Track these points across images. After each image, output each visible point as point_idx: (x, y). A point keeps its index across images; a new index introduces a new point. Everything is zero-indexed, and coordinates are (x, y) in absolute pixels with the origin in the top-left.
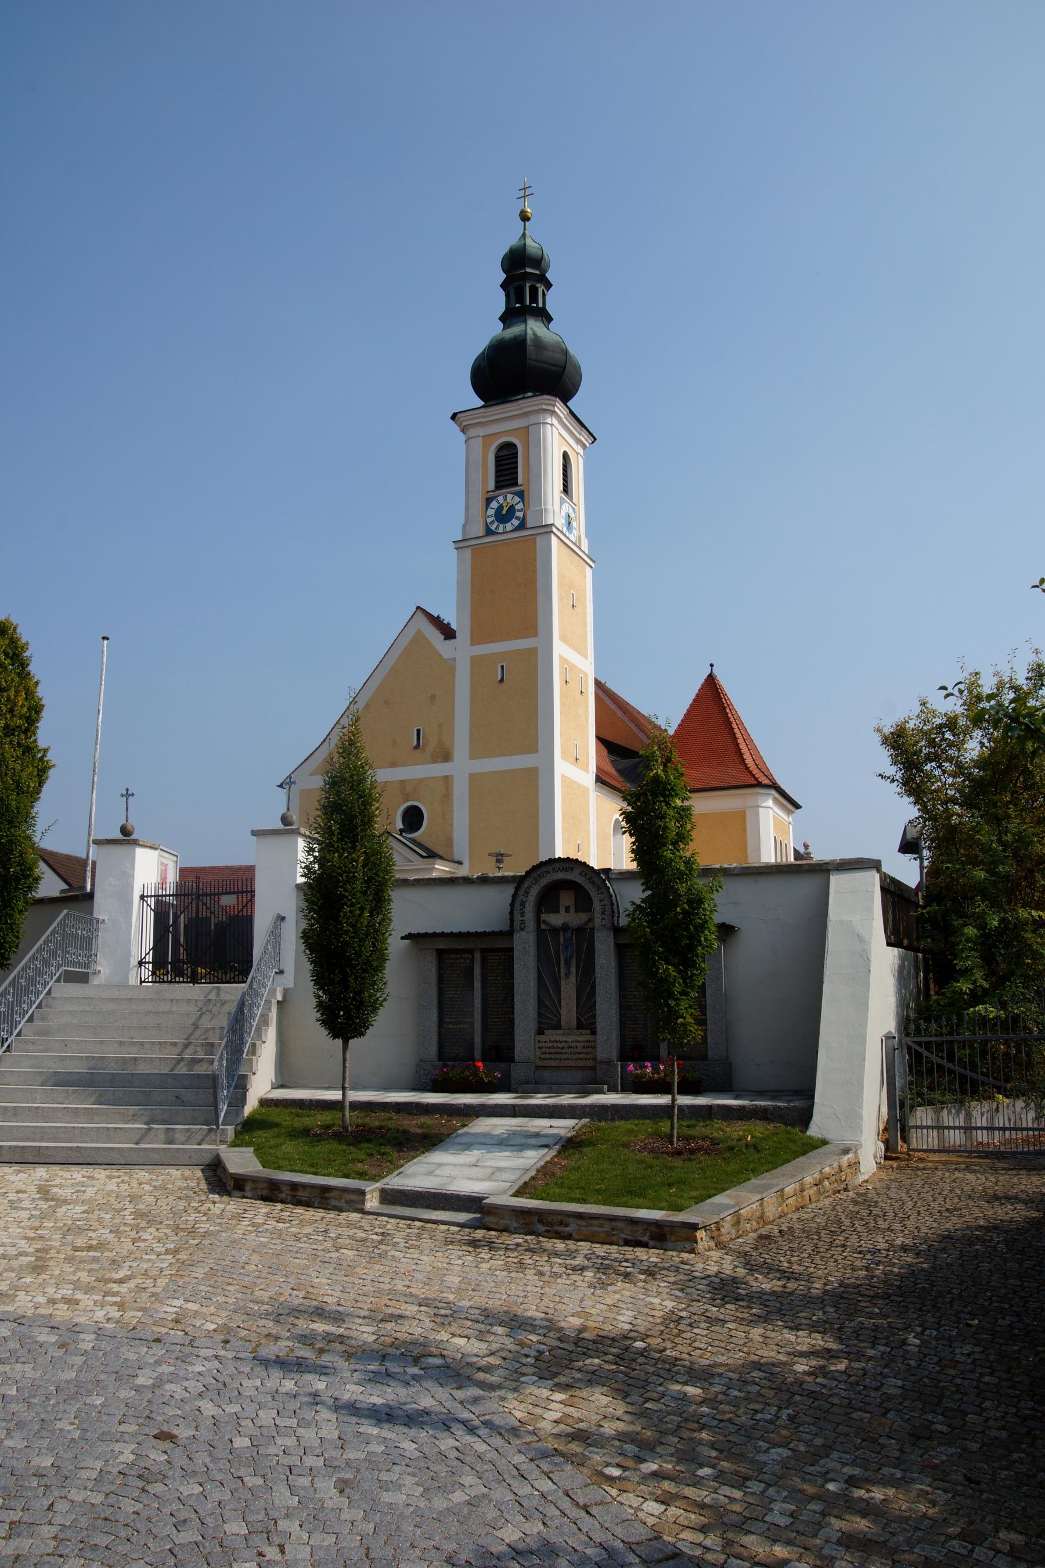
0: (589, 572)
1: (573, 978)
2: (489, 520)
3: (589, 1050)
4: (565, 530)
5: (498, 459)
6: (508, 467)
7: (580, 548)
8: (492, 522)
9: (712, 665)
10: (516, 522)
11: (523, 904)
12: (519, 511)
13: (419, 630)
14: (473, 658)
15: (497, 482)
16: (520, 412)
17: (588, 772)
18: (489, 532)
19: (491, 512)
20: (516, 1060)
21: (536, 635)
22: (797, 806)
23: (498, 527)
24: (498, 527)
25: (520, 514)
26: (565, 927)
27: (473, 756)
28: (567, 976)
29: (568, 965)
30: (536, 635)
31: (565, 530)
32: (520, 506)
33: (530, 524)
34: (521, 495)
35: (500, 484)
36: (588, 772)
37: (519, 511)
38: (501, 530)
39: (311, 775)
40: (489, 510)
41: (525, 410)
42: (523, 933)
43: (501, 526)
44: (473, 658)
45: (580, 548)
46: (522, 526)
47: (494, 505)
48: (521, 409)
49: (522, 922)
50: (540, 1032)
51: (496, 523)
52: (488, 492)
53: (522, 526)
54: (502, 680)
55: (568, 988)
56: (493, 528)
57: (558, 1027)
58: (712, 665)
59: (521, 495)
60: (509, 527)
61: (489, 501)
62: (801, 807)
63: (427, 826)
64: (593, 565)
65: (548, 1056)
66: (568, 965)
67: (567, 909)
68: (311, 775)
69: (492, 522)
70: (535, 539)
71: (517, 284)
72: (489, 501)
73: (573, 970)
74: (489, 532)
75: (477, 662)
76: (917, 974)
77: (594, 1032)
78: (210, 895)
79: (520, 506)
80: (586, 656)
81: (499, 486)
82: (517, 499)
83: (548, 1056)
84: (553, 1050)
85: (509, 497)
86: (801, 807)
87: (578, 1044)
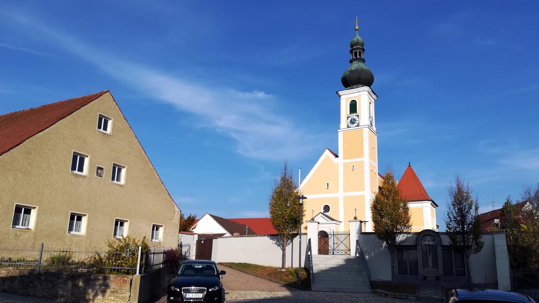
1: (431, 256)
2: (348, 123)
3: (437, 273)
4: (370, 126)
5: (351, 105)
9: (409, 163)
10: (357, 124)
11: (419, 239)
14: (363, 157)
16: (358, 91)
18: (348, 127)
19: (349, 121)
22: (437, 206)
25: (358, 122)
26: (429, 245)
27: (344, 191)
28: (430, 256)
29: (430, 253)
31: (370, 126)
32: (358, 119)
33: (361, 124)
34: (358, 116)
41: (359, 91)
42: (419, 246)
43: (352, 125)
44: (363, 157)
46: (358, 126)
47: (350, 119)
49: (419, 243)
50: (424, 268)
51: (350, 124)
53: (358, 126)
55: (430, 259)
56: (349, 126)
57: (428, 267)
58: (409, 163)
59: (358, 116)
60: (354, 125)
61: (348, 118)
62: (438, 206)
65: (426, 274)
66: (430, 253)
67: (429, 241)
70: (362, 131)
71: (355, 51)
72: (348, 118)
73: (431, 254)
74: (348, 127)
75: (345, 164)
77: (438, 269)
78: (337, 234)
82: (357, 117)
83: (426, 274)
84: (427, 272)
85: (354, 117)
86: (438, 206)
87: (434, 271)
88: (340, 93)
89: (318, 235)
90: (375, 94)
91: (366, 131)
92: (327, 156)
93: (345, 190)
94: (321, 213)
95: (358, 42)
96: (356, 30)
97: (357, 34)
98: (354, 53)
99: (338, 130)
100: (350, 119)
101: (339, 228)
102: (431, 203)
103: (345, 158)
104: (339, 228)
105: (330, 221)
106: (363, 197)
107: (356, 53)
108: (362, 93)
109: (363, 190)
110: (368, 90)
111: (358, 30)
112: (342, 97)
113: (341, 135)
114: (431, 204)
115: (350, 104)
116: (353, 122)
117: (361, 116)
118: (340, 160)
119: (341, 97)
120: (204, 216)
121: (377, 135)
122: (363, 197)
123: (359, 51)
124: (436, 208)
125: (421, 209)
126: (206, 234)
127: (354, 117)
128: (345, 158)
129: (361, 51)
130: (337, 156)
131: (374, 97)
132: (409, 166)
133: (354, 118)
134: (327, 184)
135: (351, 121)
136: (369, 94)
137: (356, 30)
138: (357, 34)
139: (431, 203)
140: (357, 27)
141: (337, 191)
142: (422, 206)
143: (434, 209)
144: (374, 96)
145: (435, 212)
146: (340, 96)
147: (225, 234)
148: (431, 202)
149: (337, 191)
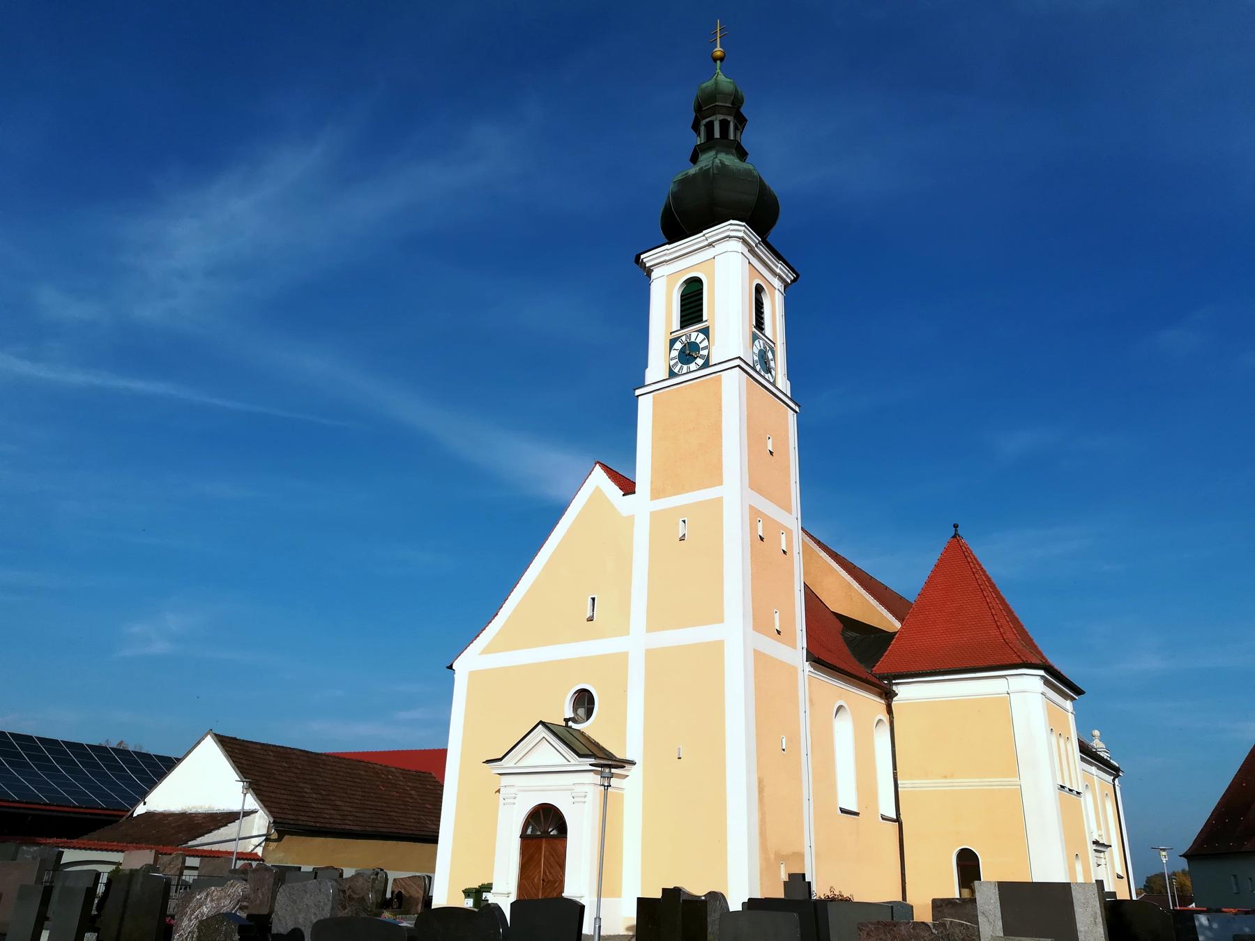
0: (792, 419)
2: (672, 363)
5: (684, 298)
6: (690, 311)
7: (774, 384)
8: (676, 364)
9: (956, 526)
10: (700, 361)
12: (703, 349)
13: (597, 487)
15: (681, 322)
16: (706, 243)
17: (794, 647)
18: (672, 374)
19: (675, 353)
20: (265, 911)
21: (721, 483)
22: (1079, 692)
23: (681, 368)
24: (681, 368)
25: (704, 352)
30: (721, 483)
31: (758, 367)
33: (712, 362)
34: (705, 332)
35: (698, 308)
36: (794, 647)
37: (703, 349)
38: (685, 370)
39: (480, 654)
40: (672, 351)
41: (710, 240)
45: (774, 384)
46: (706, 365)
47: (678, 346)
48: (704, 235)
51: (680, 365)
52: (671, 333)
54: (591, 619)
58: (956, 526)
60: (693, 366)
61: (672, 342)
63: (598, 694)
64: (797, 409)
68: (480, 654)
69: (676, 364)
70: (719, 380)
72: (672, 342)
76: (237, 905)
79: (705, 343)
80: (790, 512)
81: (684, 324)
82: (701, 336)
85: (694, 335)
88: (649, 258)
89: (146, 865)
90: (779, 257)
91: (733, 385)
92: (598, 491)
93: (654, 624)
94: (541, 723)
95: (716, 89)
96: (715, 60)
97: (718, 71)
98: (702, 129)
99: (638, 392)
100: (678, 346)
101: (624, 792)
102: (1042, 677)
103: (656, 494)
104: (624, 792)
105: (573, 762)
106: (716, 648)
107: (710, 126)
108: (720, 248)
109: (717, 617)
110: (741, 234)
111: (722, 59)
112: (654, 275)
113: (645, 406)
114: (1047, 683)
115: (681, 296)
116: (688, 354)
117: (716, 333)
118: (640, 505)
119: (653, 274)
120: (199, 743)
121: (797, 409)
122: (716, 648)
123: (721, 117)
124: (1073, 699)
125: (1003, 704)
126: (193, 811)
127: (694, 335)
128: (656, 494)
129: (730, 118)
130: (628, 487)
131: (778, 271)
132: (954, 537)
133: (693, 340)
134: (590, 601)
135: (682, 352)
136: (751, 251)
137: (715, 60)
138: (718, 71)
139: (1042, 677)
140: (718, 51)
141: (623, 630)
142: (1006, 690)
143: (1068, 705)
144: (780, 268)
145: (1071, 718)
146: (649, 271)
147: (229, 818)
148: (1042, 672)
149: (623, 630)
